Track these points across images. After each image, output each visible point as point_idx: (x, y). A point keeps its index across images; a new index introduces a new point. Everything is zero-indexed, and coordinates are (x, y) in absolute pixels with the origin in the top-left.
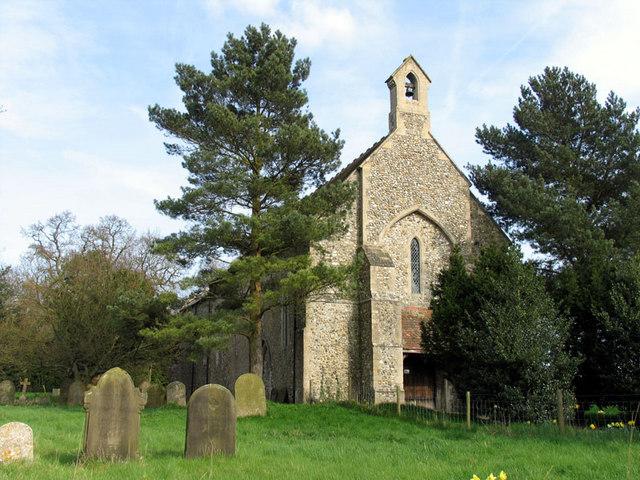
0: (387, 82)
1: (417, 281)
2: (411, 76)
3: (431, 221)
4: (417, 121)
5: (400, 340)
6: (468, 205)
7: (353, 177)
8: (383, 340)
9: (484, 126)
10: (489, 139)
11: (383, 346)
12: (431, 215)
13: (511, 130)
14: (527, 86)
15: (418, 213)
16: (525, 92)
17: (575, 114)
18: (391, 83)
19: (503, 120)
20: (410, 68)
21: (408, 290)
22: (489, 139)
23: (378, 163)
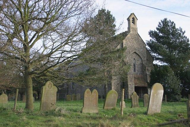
0: (127, 19)
1: (135, 69)
2: (133, 18)
3: (138, 54)
4: (136, 30)
5: (133, 83)
6: (146, 51)
7: (78, 22)
8: (130, 83)
9: (132, 19)
10: (152, 34)
11: (130, 85)
12: (138, 53)
13: (155, 32)
14: (160, 22)
15: (135, 52)
16: (160, 24)
17: (183, 39)
18: (128, 19)
19: (154, 29)
20: (133, 16)
21: (133, 71)
22: (152, 34)
23: (126, 40)
